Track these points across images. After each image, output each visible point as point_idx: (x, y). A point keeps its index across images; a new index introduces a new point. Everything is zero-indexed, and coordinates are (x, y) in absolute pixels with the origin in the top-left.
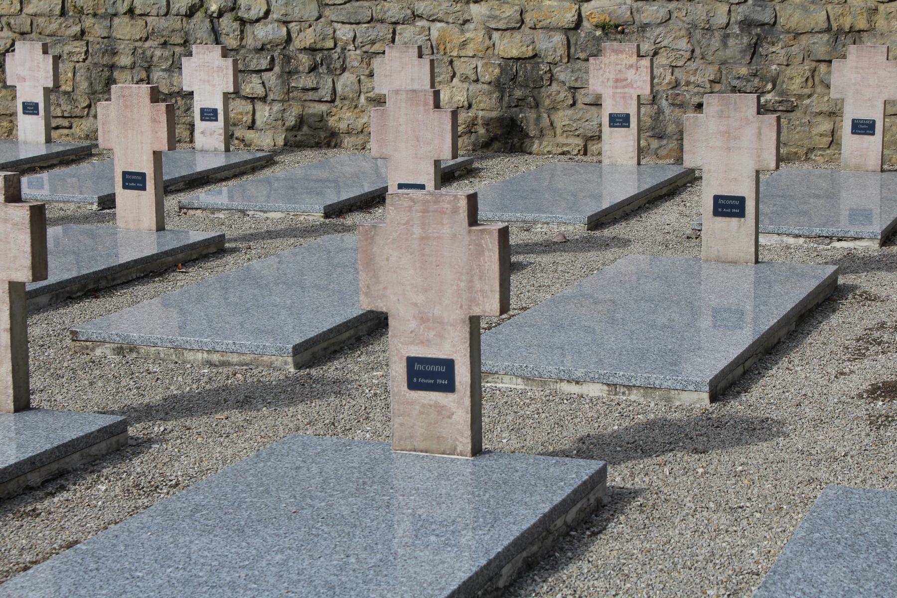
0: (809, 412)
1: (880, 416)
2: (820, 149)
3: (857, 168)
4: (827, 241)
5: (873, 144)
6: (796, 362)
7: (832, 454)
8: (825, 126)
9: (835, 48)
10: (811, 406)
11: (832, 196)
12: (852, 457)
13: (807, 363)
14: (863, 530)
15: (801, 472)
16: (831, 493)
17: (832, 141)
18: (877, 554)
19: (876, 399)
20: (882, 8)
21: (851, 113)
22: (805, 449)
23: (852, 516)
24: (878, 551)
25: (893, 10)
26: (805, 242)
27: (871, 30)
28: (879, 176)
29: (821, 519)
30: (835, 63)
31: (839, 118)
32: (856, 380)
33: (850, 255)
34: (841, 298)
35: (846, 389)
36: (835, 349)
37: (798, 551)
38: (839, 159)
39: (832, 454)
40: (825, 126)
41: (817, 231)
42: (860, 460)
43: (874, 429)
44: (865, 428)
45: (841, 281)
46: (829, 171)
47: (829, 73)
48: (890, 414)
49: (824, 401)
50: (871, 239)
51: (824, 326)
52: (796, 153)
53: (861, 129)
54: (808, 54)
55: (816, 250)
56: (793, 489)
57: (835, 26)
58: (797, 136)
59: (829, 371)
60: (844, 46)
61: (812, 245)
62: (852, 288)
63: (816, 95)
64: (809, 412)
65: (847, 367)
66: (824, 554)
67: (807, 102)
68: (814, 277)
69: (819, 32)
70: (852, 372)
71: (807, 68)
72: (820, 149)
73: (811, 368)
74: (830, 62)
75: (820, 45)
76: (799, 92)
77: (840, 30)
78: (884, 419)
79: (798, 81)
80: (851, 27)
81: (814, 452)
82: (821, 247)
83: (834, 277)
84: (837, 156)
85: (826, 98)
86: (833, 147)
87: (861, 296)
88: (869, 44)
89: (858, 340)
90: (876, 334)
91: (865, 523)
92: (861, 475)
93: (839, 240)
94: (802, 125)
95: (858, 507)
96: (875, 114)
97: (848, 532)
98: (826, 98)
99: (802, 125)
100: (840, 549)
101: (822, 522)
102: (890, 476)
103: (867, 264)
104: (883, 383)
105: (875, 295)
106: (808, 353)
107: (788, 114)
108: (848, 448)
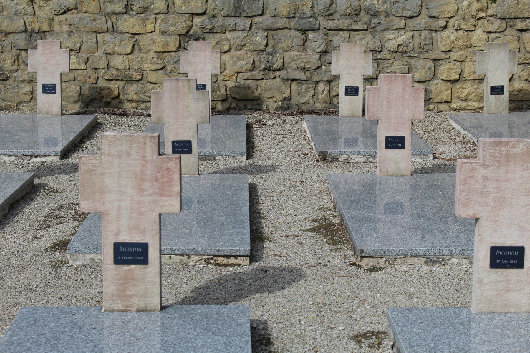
0: (15, 262)
1: (58, 261)
2: (25, 102)
3: (47, 113)
4: (29, 158)
5: (55, 99)
6: (8, 233)
7: (28, 287)
8: (27, 89)
9: (30, 42)
10: (16, 259)
11: (33, 130)
12: (40, 287)
13: (15, 233)
14: (43, 332)
15: (9, 300)
16: (25, 311)
17: (32, 98)
18: (51, 345)
19: (56, 251)
20: (56, 18)
21: (41, 81)
22: (12, 286)
23: (37, 324)
24: (52, 343)
25: (63, 19)
26: (16, 159)
27: (51, 31)
28: (60, 117)
29: (18, 328)
30: (30, 51)
31: (35, 84)
32: (45, 241)
33: (43, 166)
34: (36, 192)
35: (38, 247)
36: (32, 223)
37: (3, 350)
38: (36, 108)
39: (28, 287)
40: (27, 89)
41: (22, 152)
42: (46, 289)
43: (54, 269)
44: (48, 269)
45: (36, 181)
46: (31, 116)
47: (27, 57)
48: (64, 260)
49: (25, 255)
50: (55, 155)
51: (26, 210)
52: (10, 105)
53: (48, 90)
54: (14, 46)
55: (22, 163)
56: (4, 311)
57: (29, 29)
58: (10, 95)
59: (28, 236)
60: (35, 41)
61: (20, 160)
62: (43, 186)
63: (20, 70)
64: (15, 262)
65: (39, 233)
66: (19, 349)
67: (15, 74)
68: (20, 180)
69: (20, 32)
70: (42, 236)
71: (14, 54)
72: (25, 102)
73: (18, 235)
74: (27, 50)
75: (21, 40)
76: (10, 68)
77: (33, 31)
78: (60, 263)
79: (9, 62)
80: (39, 30)
81: (18, 287)
82: (25, 161)
83: (32, 179)
84: (35, 106)
85: (27, 72)
86: (33, 101)
87: (48, 190)
88: (50, 40)
89: (46, 217)
90: (57, 212)
91: (44, 328)
92: (46, 298)
93: (36, 157)
94: (13, 88)
95: (41, 318)
96: (56, 81)
97: (34, 334)
98: (27, 72)
99: (13, 88)
100: (29, 345)
101: (19, 330)
102: (63, 297)
103: (53, 171)
104: (60, 242)
105: (57, 189)
106: (16, 227)
107: (4, 82)
108: (38, 283)
